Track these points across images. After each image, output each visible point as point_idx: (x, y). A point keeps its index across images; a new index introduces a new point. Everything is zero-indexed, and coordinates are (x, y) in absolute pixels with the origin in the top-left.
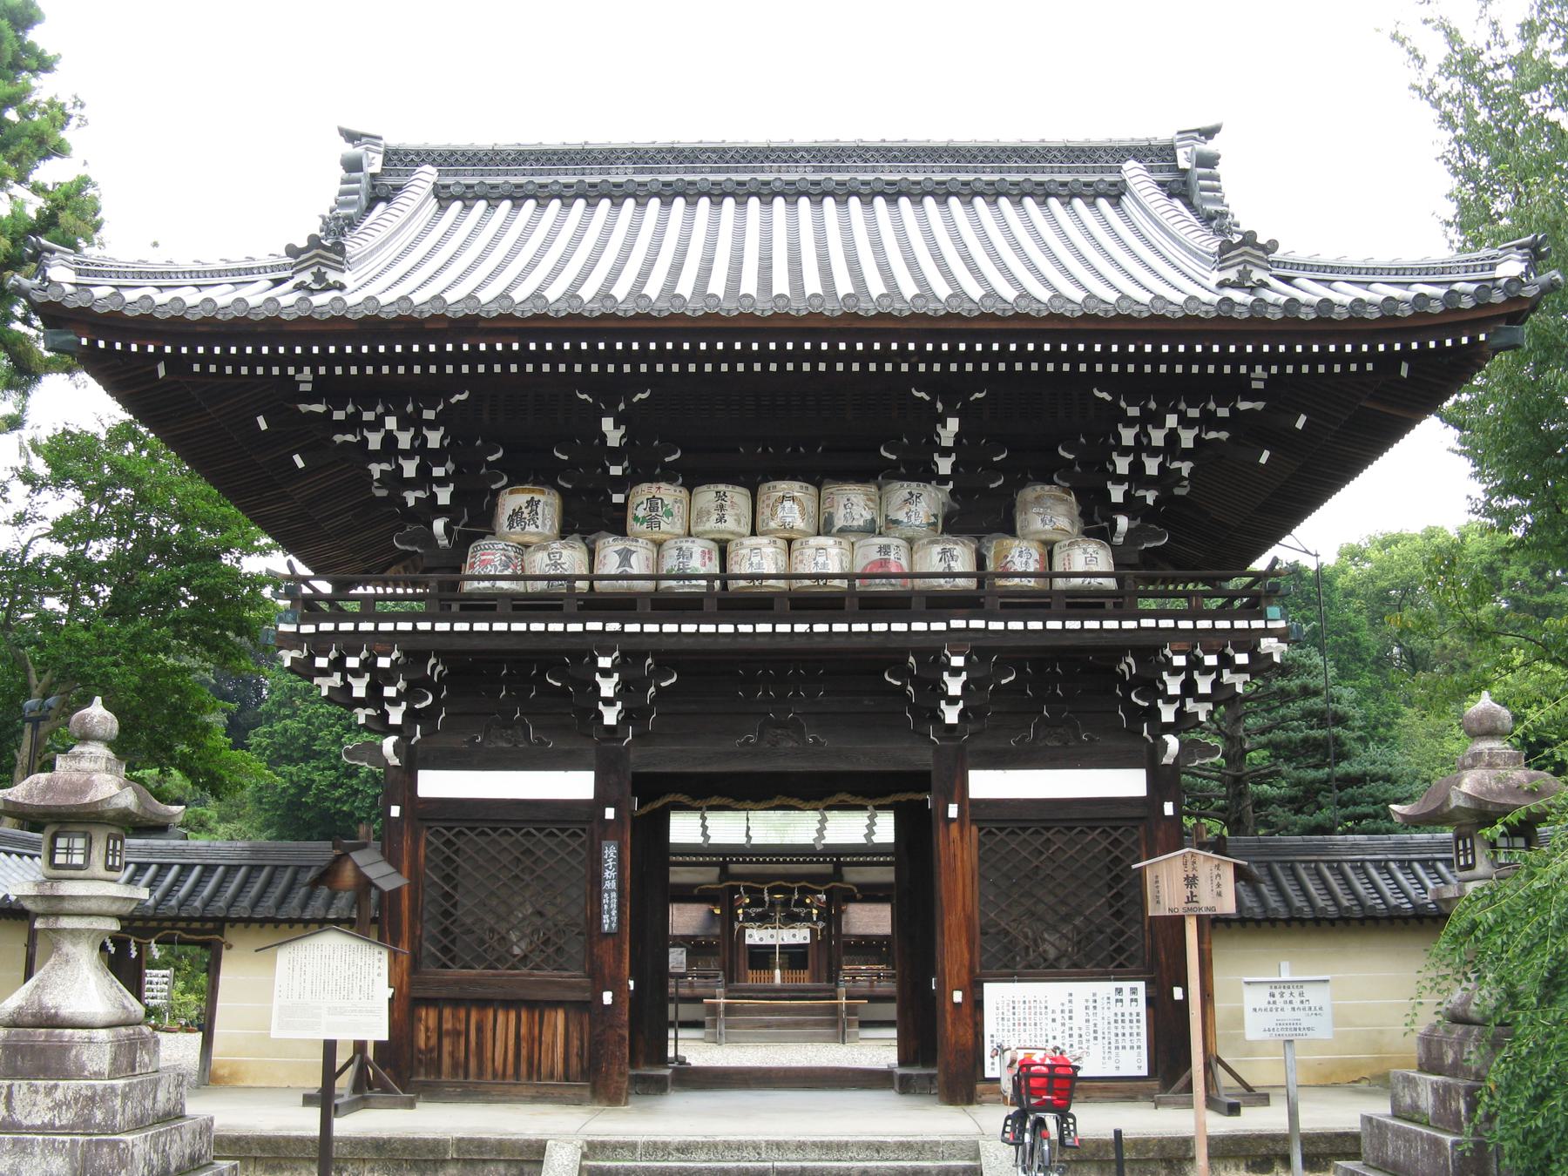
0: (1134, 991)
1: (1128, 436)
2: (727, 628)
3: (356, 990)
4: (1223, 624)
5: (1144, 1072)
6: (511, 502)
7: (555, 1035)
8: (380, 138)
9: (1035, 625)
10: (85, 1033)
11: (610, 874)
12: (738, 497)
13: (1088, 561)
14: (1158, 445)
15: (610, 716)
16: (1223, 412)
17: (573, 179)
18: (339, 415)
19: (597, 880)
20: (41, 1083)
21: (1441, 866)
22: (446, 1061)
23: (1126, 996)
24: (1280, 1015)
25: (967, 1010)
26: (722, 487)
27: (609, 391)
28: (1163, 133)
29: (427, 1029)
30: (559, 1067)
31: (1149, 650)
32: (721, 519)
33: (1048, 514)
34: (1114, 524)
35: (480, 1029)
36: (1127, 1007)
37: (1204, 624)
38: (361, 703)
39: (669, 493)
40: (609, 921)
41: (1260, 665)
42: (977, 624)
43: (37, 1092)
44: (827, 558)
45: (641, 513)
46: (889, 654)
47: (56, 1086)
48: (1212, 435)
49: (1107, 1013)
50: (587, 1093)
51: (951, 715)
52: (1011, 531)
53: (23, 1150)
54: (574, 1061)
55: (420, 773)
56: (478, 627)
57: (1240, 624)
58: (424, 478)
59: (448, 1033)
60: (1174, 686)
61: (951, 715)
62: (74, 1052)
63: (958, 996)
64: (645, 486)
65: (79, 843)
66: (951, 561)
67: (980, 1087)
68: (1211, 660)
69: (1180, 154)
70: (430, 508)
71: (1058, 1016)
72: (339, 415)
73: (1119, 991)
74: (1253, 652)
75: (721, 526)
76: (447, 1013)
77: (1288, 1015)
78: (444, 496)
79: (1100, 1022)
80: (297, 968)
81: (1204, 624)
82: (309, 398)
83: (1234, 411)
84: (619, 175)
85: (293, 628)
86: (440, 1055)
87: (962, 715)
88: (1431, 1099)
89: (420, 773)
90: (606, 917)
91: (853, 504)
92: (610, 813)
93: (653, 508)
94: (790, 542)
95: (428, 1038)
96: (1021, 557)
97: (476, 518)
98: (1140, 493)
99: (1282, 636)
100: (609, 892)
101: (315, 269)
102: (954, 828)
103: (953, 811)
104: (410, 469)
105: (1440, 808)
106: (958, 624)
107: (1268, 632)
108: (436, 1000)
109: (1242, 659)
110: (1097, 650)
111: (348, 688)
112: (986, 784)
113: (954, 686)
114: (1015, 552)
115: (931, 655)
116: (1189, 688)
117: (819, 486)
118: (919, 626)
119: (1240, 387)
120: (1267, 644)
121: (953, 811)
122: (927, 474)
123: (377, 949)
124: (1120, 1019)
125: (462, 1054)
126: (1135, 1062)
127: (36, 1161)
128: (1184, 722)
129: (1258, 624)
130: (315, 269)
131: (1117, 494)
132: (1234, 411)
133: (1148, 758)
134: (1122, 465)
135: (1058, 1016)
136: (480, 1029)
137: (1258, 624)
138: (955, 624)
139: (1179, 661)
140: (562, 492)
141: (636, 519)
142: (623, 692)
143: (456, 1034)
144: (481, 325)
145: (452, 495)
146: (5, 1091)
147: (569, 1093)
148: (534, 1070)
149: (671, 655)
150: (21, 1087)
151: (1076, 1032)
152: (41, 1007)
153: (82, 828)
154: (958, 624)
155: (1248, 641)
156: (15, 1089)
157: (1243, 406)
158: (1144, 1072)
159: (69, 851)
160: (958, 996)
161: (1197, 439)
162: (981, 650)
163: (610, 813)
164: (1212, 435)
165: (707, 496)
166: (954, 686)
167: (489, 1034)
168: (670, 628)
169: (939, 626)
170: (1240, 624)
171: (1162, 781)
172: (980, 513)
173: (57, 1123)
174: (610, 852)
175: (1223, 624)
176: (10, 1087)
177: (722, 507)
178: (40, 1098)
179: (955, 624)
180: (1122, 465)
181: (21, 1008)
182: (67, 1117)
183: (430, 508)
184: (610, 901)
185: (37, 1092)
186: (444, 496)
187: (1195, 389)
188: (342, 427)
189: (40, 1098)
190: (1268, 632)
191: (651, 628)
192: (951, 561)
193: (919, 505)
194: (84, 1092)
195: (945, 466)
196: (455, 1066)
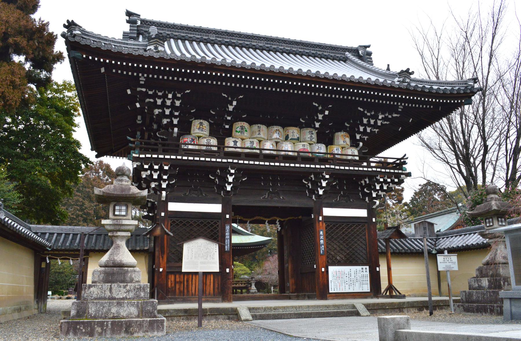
0: (366, 269)
3: (209, 256)
4: (392, 171)
5: (369, 291)
6: (196, 123)
7: (210, 282)
8: (140, 16)
9: (347, 168)
10: (132, 269)
12: (263, 127)
13: (353, 152)
14: (373, 123)
16: (390, 117)
17: (199, 37)
18: (150, 93)
20: (122, 284)
21: (413, 240)
22: (177, 290)
23: (364, 270)
24: (446, 264)
25: (325, 273)
26: (259, 125)
27: (234, 93)
28: (355, 45)
29: (171, 281)
32: (259, 134)
33: (342, 140)
34: (359, 144)
35: (187, 281)
36: (365, 273)
37: (388, 171)
38: (155, 180)
39: (246, 125)
43: (120, 287)
44: (287, 146)
45: (238, 130)
46: (306, 173)
47: (127, 285)
48: (385, 122)
49: (360, 275)
50: (220, 299)
51: (229, 188)
53: (121, 305)
54: (216, 290)
56: (196, 159)
57: (396, 171)
58: (171, 115)
59: (178, 282)
62: (129, 275)
63: (323, 270)
64: (239, 123)
65: (124, 208)
66: (321, 148)
67: (328, 295)
70: (171, 125)
71: (347, 275)
72: (150, 93)
73: (362, 269)
75: (259, 136)
76: (177, 276)
77: (448, 264)
78: (175, 121)
80: (190, 250)
81: (388, 171)
82: (142, 86)
83: (392, 116)
84: (213, 37)
85: (138, 156)
86: (175, 289)
88: (487, 283)
90: (226, 246)
91: (293, 132)
92: (228, 216)
93: (242, 129)
95: (171, 284)
97: (186, 129)
98: (364, 137)
100: (227, 239)
101: (155, 45)
102: (321, 223)
103: (321, 218)
104: (167, 112)
105: (489, 209)
108: (174, 272)
110: (355, 175)
111: (151, 175)
113: (231, 179)
114: (335, 149)
119: (394, 109)
121: (321, 218)
123: (215, 244)
124: (363, 276)
125: (182, 289)
126: (367, 288)
127: (125, 309)
130: (155, 45)
132: (392, 116)
134: (361, 129)
135: (347, 275)
136: (187, 281)
141: (237, 131)
143: (180, 282)
144: (215, 67)
145: (178, 121)
146: (109, 287)
147: (215, 299)
150: (115, 286)
151: (352, 280)
152: (114, 260)
153: (125, 203)
156: (113, 286)
157: (395, 115)
158: (369, 291)
159: (120, 210)
160: (323, 270)
161: (381, 123)
163: (228, 216)
164: (385, 122)
165: (255, 127)
167: (190, 283)
169: (323, 167)
173: (128, 297)
175: (392, 171)
176: (111, 286)
177: (259, 131)
178: (122, 289)
180: (361, 129)
181: (107, 261)
182: (131, 295)
183: (171, 125)
185: (120, 287)
186: (175, 121)
187: (384, 109)
188: (150, 97)
189: (122, 289)
194: (137, 287)
195: (317, 125)
196: (180, 292)
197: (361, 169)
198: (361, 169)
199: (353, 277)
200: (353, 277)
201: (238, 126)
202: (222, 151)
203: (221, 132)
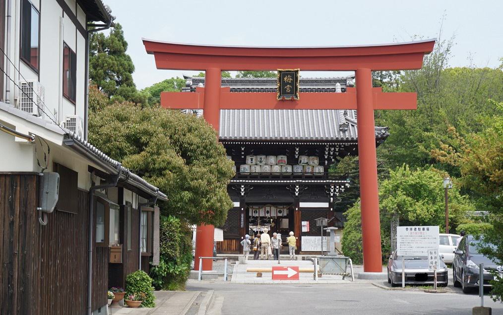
1: (327, 149)
2: (262, 181)
11: (242, 219)
13: (320, 170)
15: (243, 194)
19: (240, 220)
30: (234, 249)
31: (329, 185)
40: (242, 226)
41: (345, 187)
42: (301, 181)
51: (297, 194)
55: (300, 203)
57: (342, 181)
60: (332, 191)
68: (338, 187)
74: (345, 186)
87: (244, 194)
89: (300, 203)
92: (242, 209)
94: (271, 166)
99: (349, 183)
102: (297, 212)
103: (297, 209)
106: (298, 181)
109: (343, 187)
112: (303, 205)
113: (297, 190)
115: (294, 186)
116: (335, 191)
118: (291, 181)
120: (347, 185)
121: (297, 209)
131: (326, 157)
133: (329, 201)
138: (297, 181)
139: (333, 187)
140: (287, 156)
142: (244, 190)
148: (230, 249)
149: (252, 185)
154: (298, 181)
155: (344, 184)
163: (242, 209)
168: (307, 181)
170: (342, 181)
171: (330, 204)
174: (242, 215)
179: (297, 181)
184: (242, 223)
191: (282, 181)
199: (317, 242)
200: (317, 242)
201: (249, 158)
202: (239, 176)
203: (239, 161)
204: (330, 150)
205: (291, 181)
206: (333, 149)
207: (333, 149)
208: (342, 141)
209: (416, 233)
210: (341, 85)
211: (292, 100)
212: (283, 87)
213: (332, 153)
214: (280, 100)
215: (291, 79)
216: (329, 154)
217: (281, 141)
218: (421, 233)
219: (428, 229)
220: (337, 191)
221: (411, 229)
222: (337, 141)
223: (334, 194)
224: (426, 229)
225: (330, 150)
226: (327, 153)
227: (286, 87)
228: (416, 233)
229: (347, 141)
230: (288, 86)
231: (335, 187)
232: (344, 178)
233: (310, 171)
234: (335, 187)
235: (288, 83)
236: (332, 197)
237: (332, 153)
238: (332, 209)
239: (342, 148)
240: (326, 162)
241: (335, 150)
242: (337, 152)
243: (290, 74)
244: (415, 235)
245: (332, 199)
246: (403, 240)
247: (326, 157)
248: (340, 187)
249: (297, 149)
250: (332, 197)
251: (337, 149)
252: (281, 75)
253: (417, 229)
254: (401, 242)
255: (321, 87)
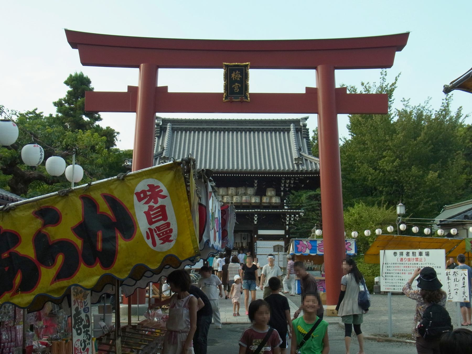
1: (283, 181)
12: (225, 189)
13: (276, 200)
31: (284, 214)
33: (270, 192)
41: (300, 216)
42: (259, 210)
51: (256, 223)
52: (265, 195)
57: (297, 211)
60: (288, 219)
61: (256, 223)
68: (293, 216)
69: (301, 123)
79: (410, 269)
81: (292, 211)
89: (127, 91)
91: (241, 190)
96: (265, 200)
103: (256, 236)
106: (256, 210)
107: (301, 212)
109: (297, 216)
113: (256, 219)
116: (290, 219)
117: (227, 188)
118: (250, 211)
121: (256, 236)
122: (252, 186)
128: (290, 224)
129: (300, 211)
131: (282, 189)
133: (285, 229)
137: (300, 211)
139: (288, 216)
154: (256, 210)
155: (298, 213)
162: (259, 214)
166: (256, 219)
169: (253, 211)
170: (297, 211)
172: (261, 193)
175: (295, 211)
190: (301, 212)
192: (254, 200)
193: (250, 191)
195: (256, 185)
197: (284, 210)
198: (284, 210)
204: (285, 182)
205: (250, 211)
206: (288, 181)
207: (288, 181)
208: (297, 173)
209: (409, 260)
210: (296, 125)
211: (242, 102)
212: (231, 86)
213: (287, 185)
214: (227, 102)
215: (239, 76)
216: (285, 186)
217: (241, 172)
218: (417, 259)
219: (427, 254)
220: (292, 219)
221: (401, 254)
222: (293, 172)
223: (289, 223)
224: (424, 254)
225: (285, 182)
226: (283, 185)
227: (233, 86)
228: (409, 260)
229: (302, 173)
230: (237, 84)
231: (290, 216)
232: (299, 208)
233: (268, 201)
234: (290, 216)
235: (236, 81)
236: (287, 225)
237: (287, 185)
238: (287, 236)
239: (297, 180)
240: (282, 193)
241: (290, 183)
242: (292, 184)
243: (239, 70)
244: (407, 262)
245: (287, 227)
246: (389, 269)
247: (282, 189)
248: (295, 216)
249: (256, 181)
250: (287, 225)
251: (292, 182)
252: (227, 70)
253: (411, 254)
254: (387, 272)
255: (277, 127)
